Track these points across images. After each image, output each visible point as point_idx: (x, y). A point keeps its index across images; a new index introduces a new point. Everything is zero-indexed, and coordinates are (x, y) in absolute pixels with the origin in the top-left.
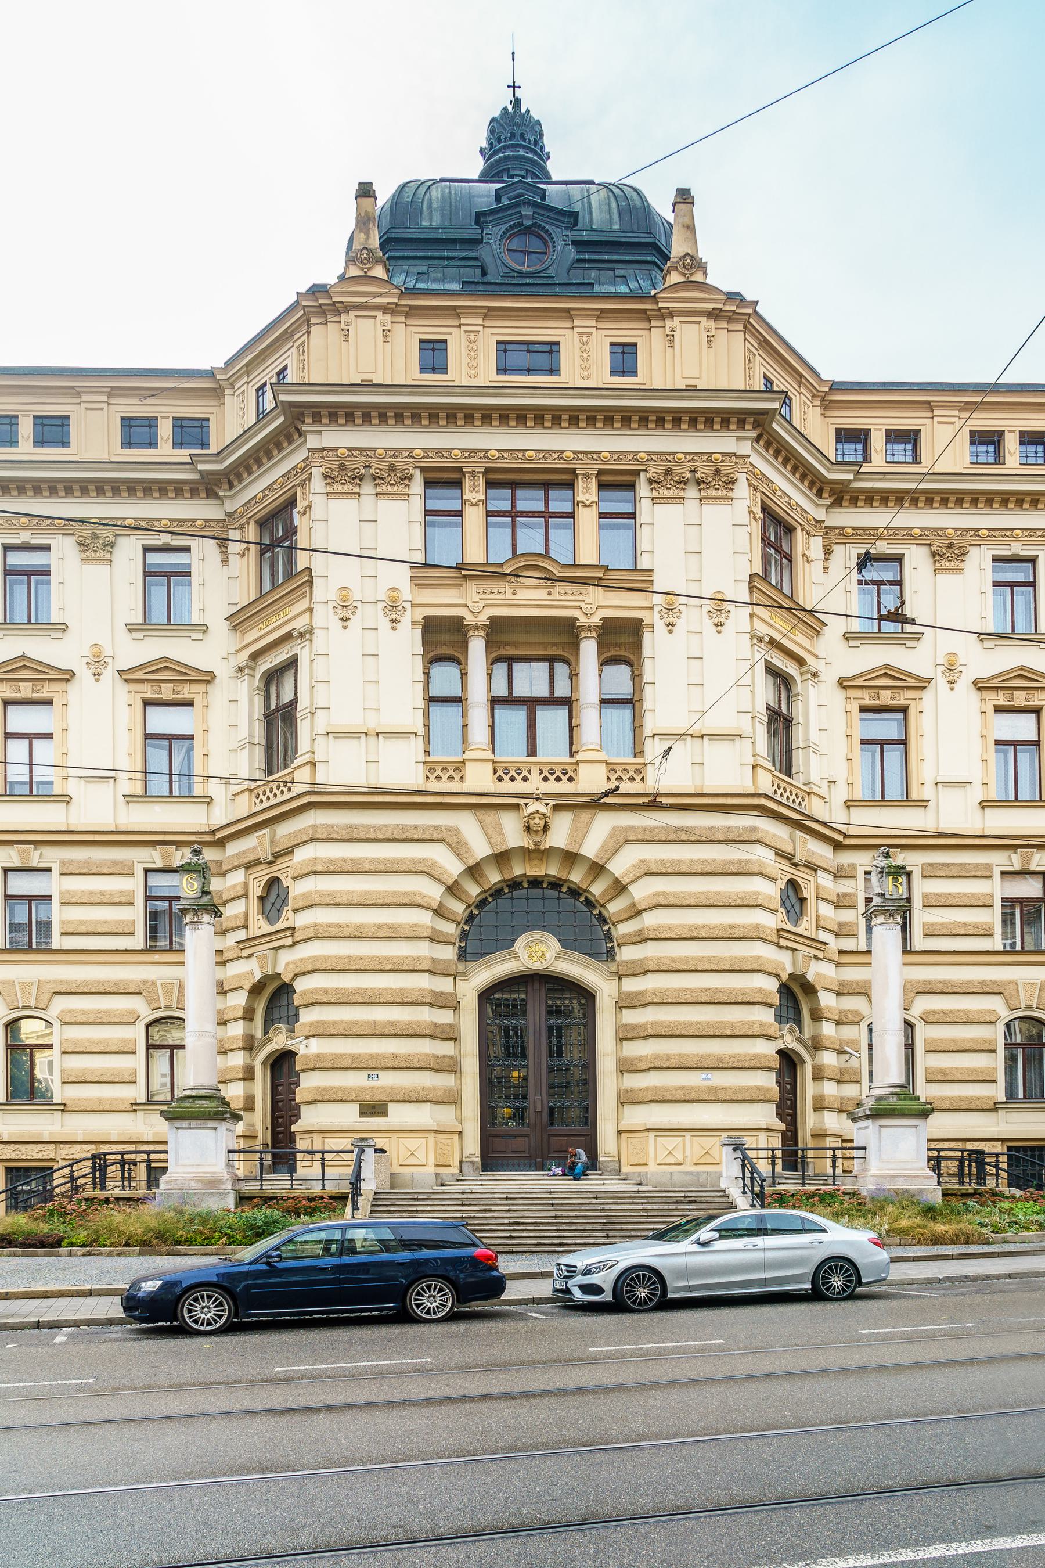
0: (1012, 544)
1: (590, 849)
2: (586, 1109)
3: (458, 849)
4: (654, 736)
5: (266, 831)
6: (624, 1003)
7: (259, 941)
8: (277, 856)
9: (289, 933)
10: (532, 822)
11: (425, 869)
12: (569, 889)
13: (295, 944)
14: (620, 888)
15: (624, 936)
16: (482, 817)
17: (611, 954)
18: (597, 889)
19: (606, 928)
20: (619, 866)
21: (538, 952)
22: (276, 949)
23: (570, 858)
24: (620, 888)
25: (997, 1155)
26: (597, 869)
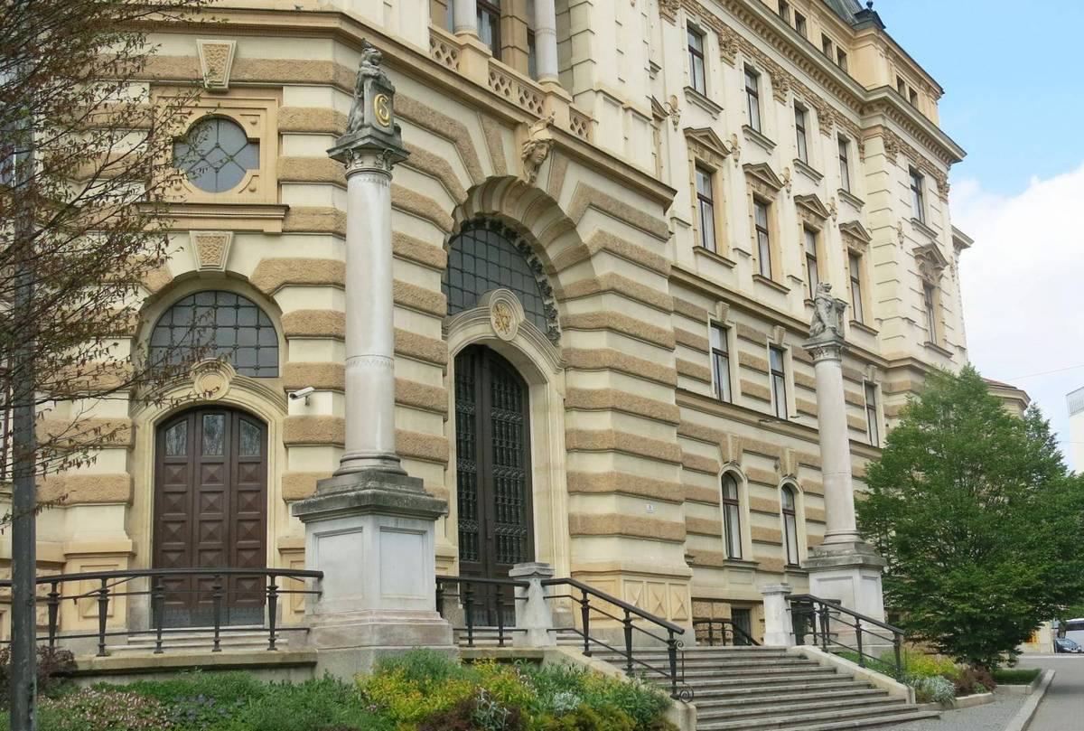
0: (697, 16)
1: (565, 204)
2: (29, 540)
3: (470, 163)
4: (597, 92)
5: (230, 42)
6: (576, 403)
7: (195, 212)
8: (236, 85)
9: (281, 213)
10: (538, 151)
11: (441, 173)
12: (522, 244)
13: (285, 232)
14: (583, 256)
15: (576, 317)
16: (488, 126)
17: (553, 336)
18: (553, 252)
19: (547, 302)
20: (591, 228)
21: (503, 321)
22: (237, 232)
23: (547, 204)
24: (583, 256)
25: (723, 621)
26: (567, 227)
